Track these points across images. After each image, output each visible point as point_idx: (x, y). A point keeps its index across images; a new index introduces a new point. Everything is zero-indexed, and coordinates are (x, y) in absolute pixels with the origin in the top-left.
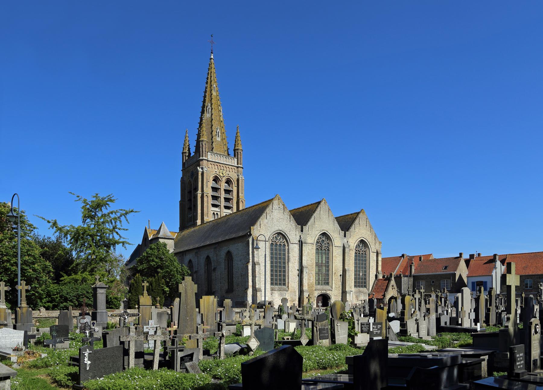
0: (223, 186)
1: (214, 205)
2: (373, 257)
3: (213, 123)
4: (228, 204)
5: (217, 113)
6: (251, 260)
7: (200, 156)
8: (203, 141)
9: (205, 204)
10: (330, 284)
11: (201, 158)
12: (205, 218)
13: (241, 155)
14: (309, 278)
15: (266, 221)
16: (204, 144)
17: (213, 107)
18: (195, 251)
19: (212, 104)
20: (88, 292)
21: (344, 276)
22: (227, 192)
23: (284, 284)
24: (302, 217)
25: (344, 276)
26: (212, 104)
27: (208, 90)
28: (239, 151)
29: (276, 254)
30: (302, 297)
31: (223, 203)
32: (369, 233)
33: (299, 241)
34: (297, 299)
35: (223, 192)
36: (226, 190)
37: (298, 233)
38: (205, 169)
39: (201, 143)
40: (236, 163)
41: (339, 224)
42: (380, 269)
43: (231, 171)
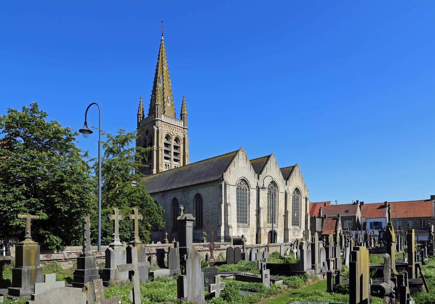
0: (173, 143)
1: (166, 158)
2: (303, 201)
3: (164, 91)
4: (176, 158)
5: (166, 84)
6: (223, 201)
7: (155, 117)
8: (158, 105)
9: (160, 157)
10: (276, 222)
11: (156, 119)
12: (160, 168)
13: (187, 119)
14: (264, 217)
15: (234, 168)
16: (159, 107)
17: (164, 78)
18: (161, 194)
19: (163, 76)
20: (126, 227)
21: (286, 216)
22: (176, 147)
23: (246, 222)
24: (259, 166)
25: (286, 216)
26: (163, 76)
27: (160, 64)
28: (185, 116)
29: (241, 196)
30: (259, 233)
31: (173, 157)
32: (301, 182)
33: (257, 187)
34: (255, 235)
35: (173, 148)
36: (175, 147)
37: (256, 180)
38: (160, 128)
39: (156, 106)
40: (183, 125)
41: (282, 173)
42: (308, 211)
43: (179, 131)
